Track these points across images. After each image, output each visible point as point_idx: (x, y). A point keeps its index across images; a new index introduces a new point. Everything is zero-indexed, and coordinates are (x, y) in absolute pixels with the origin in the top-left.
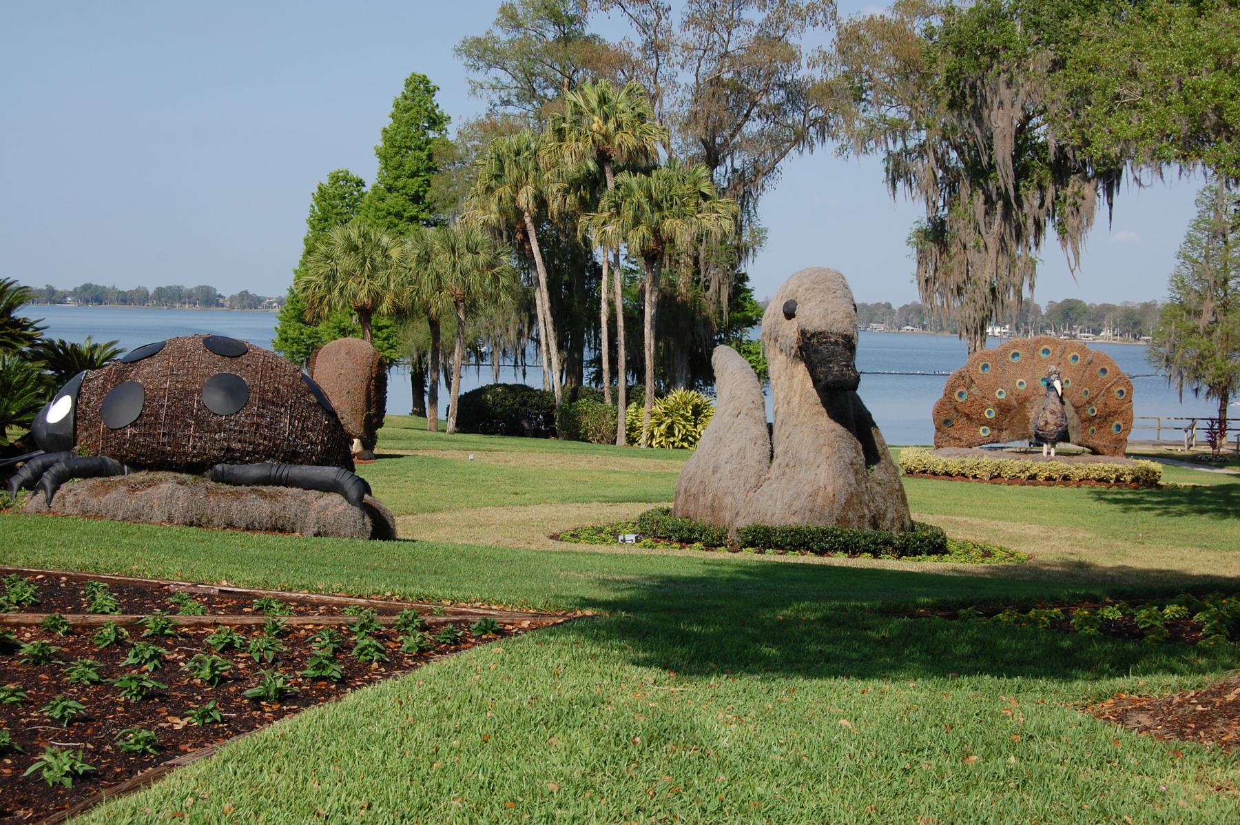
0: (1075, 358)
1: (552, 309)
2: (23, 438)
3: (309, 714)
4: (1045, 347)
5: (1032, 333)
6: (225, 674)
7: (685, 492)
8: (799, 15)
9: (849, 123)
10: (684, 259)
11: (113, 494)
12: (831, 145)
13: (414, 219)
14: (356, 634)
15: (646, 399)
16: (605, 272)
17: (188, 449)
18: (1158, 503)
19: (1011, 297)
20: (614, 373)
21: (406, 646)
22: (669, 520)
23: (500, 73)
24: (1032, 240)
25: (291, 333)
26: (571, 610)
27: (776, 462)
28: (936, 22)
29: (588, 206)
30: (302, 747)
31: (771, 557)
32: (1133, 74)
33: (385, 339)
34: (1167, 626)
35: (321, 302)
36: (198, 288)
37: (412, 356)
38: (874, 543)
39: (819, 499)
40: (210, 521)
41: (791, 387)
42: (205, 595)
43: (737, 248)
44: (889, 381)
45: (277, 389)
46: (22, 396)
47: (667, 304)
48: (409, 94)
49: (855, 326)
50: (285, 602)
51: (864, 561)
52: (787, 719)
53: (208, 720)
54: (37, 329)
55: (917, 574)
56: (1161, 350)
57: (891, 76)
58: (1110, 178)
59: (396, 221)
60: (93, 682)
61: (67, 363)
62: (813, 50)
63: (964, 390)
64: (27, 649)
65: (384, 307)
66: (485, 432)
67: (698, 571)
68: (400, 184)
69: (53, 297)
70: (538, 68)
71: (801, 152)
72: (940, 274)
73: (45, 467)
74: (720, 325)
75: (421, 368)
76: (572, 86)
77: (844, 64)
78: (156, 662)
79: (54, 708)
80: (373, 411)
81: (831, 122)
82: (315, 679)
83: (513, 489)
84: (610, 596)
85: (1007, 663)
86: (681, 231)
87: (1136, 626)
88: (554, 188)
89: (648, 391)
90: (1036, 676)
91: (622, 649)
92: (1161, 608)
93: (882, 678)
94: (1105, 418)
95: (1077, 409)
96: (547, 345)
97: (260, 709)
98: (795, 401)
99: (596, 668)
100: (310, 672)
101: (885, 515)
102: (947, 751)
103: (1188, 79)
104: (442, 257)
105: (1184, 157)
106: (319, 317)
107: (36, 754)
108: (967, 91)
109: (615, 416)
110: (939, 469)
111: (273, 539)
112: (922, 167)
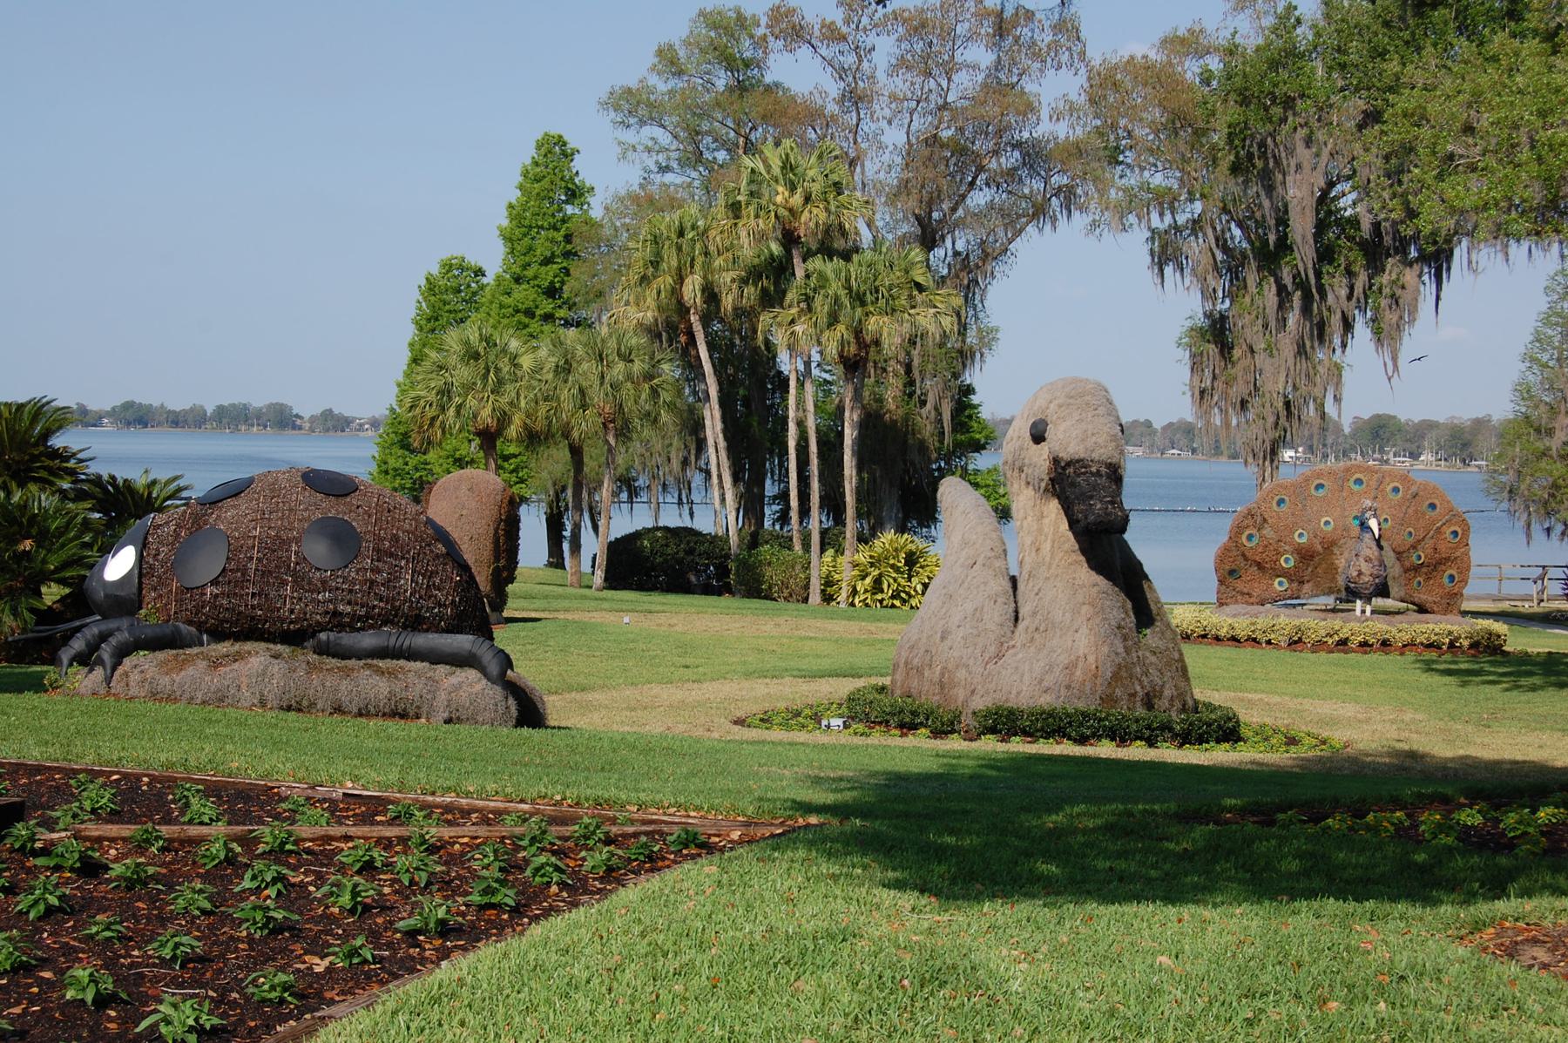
0: (1396, 490)
1: (725, 431)
2: (63, 600)
3: (487, 952)
4: (1357, 476)
5: (1332, 458)
6: (368, 901)
7: (906, 663)
8: (1036, 55)
9: (1102, 193)
10: (893, 366)
11: (190, 671)
12: (1080, 220)
13: (548, 318)
14: (525, 849)
15: (847, 544)
16: (793, 383)
17: (284, 612)
18: (1504, 675)
19: (1311, 411)
20: (804, 512)
21: (588, 864)
22: (886, 700)
23: (657, 132)
24: (1337, 341)
25: (392, 463)
26: (790, 817)
27: (1022, 625)
28: (1214, 64)
29: (772, 299)
30: (486, 995)
31: (1019, 746)
32: (1469, 129)
33: (512, 472)
34: (1543, 833)
35: (431, 425)
36: (271, 406)
37: (547, 492)
38: (1149, 727)
39: (1078, 673)
40: (312, 705)
41: (1040, 530)
42: (325, 800)
43: (961, 352)
44: (1159, 520)
45: (395, 538)
46: (63, 546)
47: (872, 423)
48: (541, 160)
49: (1122, 453)
50: (428, 808)
51: (1137, 752)
52: (1089, 955)
53: (355, 961)
54: (81, 461)
55: (1208, 767)
56: (1503, 478)
57: (1157, 132)
58: (1438, 259)
59: (527, 320)
60: (204, 912)
61: (123, 506)
62: (1055, 100)
63: (1254, 531)
64: (117, 869)
65: (513, 431)
66: (641, 587)
67: (932, 766)
68: (530, 273)
69: (86, 418)
70: (705, 126)
71: (1041, 230)
72: (1219, 384)
73: (103, 637)
74: (939, 450)
75: (558, 507)
76: (750, 148)
77: (1097, 117)
78: (279, 885)
79: (163, 945)
80: (502, 563)
81: (1079, 191)
82: (482, 908)
83: (683, 661)
84: (830, 798)
85: (1347, 882)
86: (888, 331)
87: (1503, 834)
88: (727, 277)
89: (848, 535)
90: (1394, 899)
91: (865, 868)
92: (1534, 811)
93: (1197, 902)
94: (1435, 566)
95: (1399, 555)
96: (720, 476)
97: (419, 946)
98: (1046, 547)
99: (838, 892)
100: (476, 898)
101: (1161, 692)
102: (1298, 997)
103: (1541, 133)
104: (585, 366)
105: (1538, 233)
106: (429, 443)
107: (146, 1004)
108: (1255, 149)
109: (806, 566)
110: (1223, 632)
111: (394, 727)
112: (1196, 248)
